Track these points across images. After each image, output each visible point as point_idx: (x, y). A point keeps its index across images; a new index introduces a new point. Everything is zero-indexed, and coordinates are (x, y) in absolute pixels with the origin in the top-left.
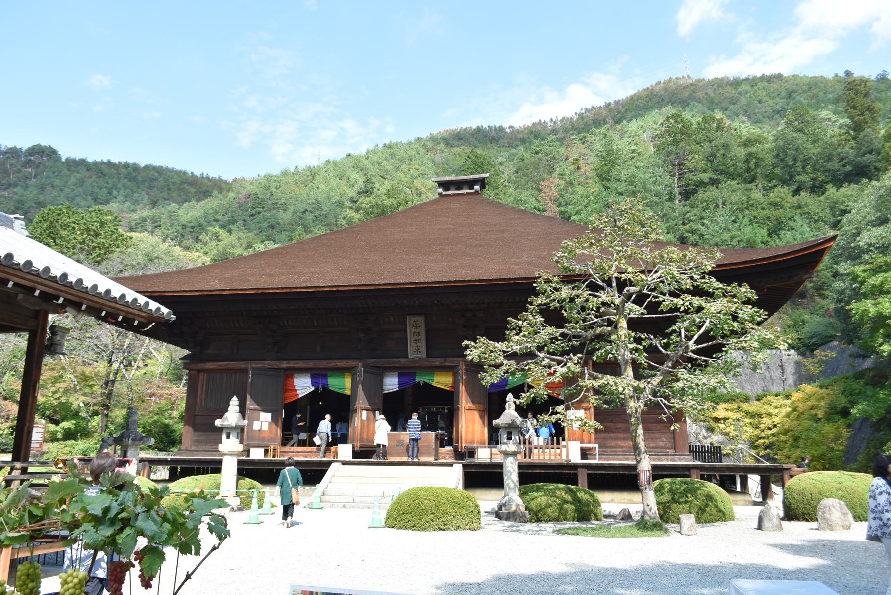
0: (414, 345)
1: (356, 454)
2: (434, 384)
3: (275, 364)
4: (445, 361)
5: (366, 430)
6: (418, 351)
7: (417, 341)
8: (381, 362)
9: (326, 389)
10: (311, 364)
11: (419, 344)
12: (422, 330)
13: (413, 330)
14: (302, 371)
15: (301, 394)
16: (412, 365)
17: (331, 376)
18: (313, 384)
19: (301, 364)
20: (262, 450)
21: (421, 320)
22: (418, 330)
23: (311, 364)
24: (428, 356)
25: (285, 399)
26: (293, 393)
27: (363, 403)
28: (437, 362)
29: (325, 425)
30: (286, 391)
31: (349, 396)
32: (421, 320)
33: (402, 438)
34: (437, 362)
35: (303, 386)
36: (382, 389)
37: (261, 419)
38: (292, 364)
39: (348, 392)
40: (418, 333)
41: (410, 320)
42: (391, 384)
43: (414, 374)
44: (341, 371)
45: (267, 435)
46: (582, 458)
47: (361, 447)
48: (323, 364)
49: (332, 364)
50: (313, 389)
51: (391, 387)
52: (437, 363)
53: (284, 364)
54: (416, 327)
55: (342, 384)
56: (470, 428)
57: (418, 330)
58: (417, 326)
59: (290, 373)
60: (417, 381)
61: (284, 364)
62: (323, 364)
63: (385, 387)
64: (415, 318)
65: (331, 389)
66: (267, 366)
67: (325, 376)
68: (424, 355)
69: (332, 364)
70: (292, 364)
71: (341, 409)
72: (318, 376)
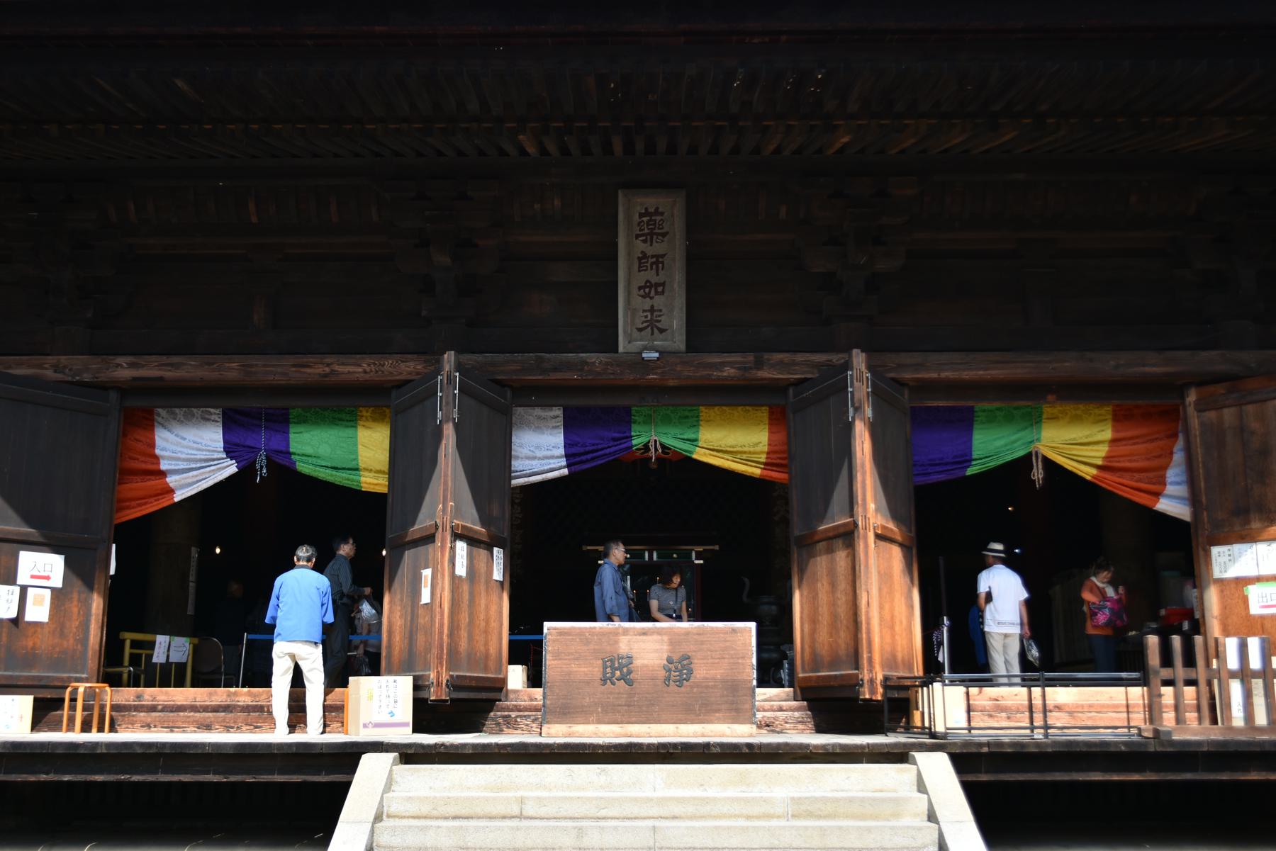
0: (642, 304)
1: (427, 715)
2: (701, 455)
3: (85, 367)
4: (759, 364)
5: (464, 617)
6: (653, 325)
7: (650, 289)
8: (510, 365)
9: (283, 470)
10: (230, 369)
11: (659, 301)
12: (674, 249)
13: (640, 246)
14: (188, 399)
15: (184, 487)
16: (629, 377)
17: (302, 421)
18: (230, 450)
19: (190, 369)
20: (25, 704)
21: (672, 208)
22: (657, 248)
23: (230, 369)
24: (693, 345)
25: (121, 504)
26: (153, 483)
27: (458, 512)
28: (728, 367)
29: (301, 594)
30: (128, 474)
31: (376, 500)
32: (672, 208)
33: (624, 647)
34: (728, 367)
35: (193, 457)
36: (507, 472)
37: (23, 578)
38: (151, 369)
39: (374, 482)
40: (658, 261)
41: (630, 209)
42: (540, 452)
43: (623, 419)
44: (342, 403)
45: (43, 643)
46: (416, 730)
47: (455, 685)
48: (279, 369)
49: (317, 369)
50: (230, 468)
51: (536, 465)
52: (729, 371)
53: (124, 370)
54: (650, 237)
55: (361, 453)
56: (887, 606)
57: (657, 248)
58: (652, 229)
59: (143, 408)
60: (637, 442)
61: (124, 370)
62: (279, 369)
63: (516, 465)
64: (650, 201)
65: (304, 467)
66: (50, 374)
67: (280, 422)
68: (677, 340)
69: (317, 369)
70: (151, 369)
71: (364, 540)
72: (251, 418)
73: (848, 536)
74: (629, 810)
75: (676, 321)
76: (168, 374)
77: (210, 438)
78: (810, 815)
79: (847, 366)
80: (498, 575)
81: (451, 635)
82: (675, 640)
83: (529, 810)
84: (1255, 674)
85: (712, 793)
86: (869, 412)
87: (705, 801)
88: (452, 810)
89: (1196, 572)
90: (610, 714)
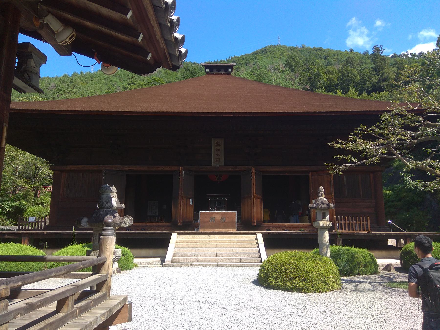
52: (231, 169)
66: (114, 169)
68: (223, 164)
73: (250, 197)
74: (213, 242)
75: (222, 160)
76: (135, 169)
77: (394, 241)
78: (240, 243)
79: (251, 170)
80: (191, 203)
81: (183, 214)
82: (223, 214)
83: (198, 242)
84: (40, 222)
85: (226, 239)
86: (255, 178)
87: (225, 240)
88: (187, 242)
89: (287, 97)
90: (212, 227)
